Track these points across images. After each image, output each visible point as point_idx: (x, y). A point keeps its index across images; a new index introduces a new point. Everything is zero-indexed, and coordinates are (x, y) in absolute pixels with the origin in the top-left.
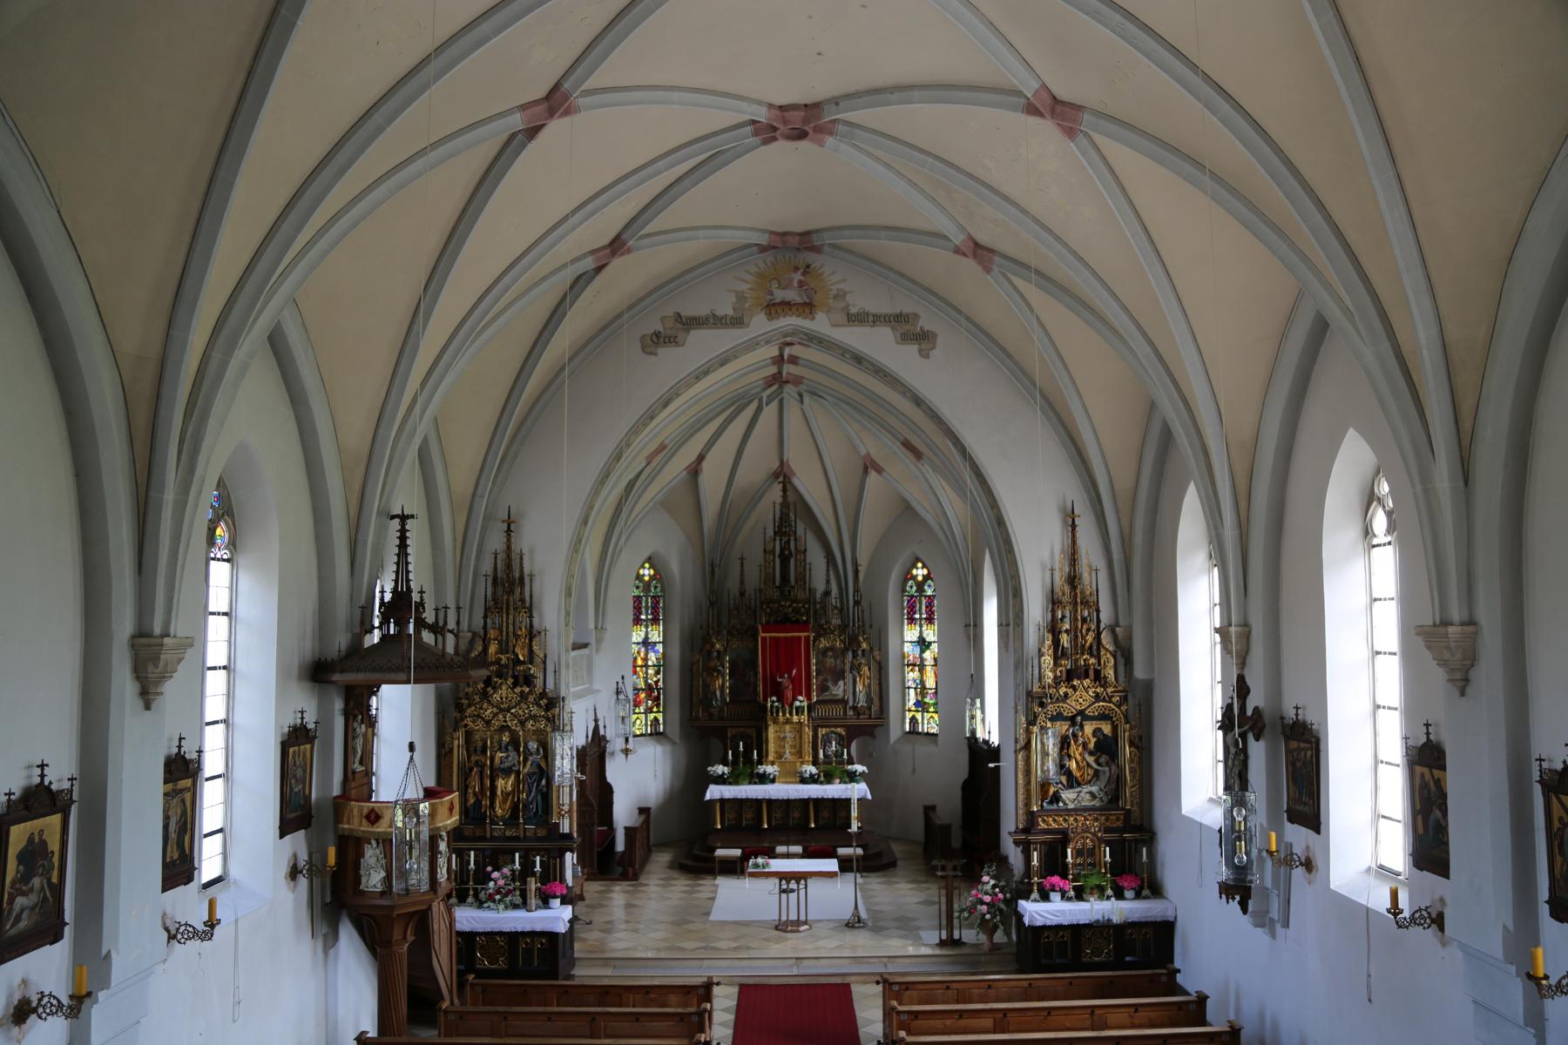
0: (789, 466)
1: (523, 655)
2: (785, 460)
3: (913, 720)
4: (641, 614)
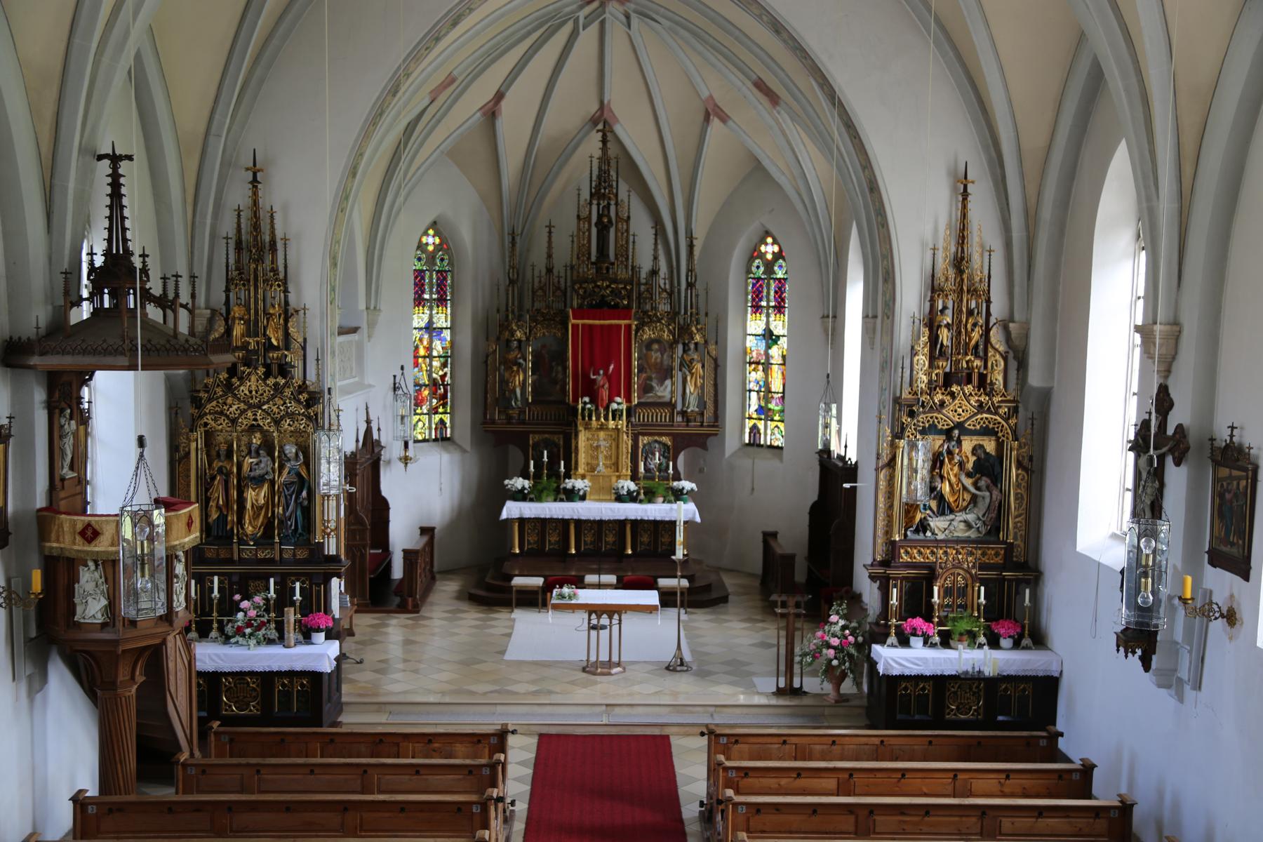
1: (277, 340)
2: (606, 102)
4: (423, 292)
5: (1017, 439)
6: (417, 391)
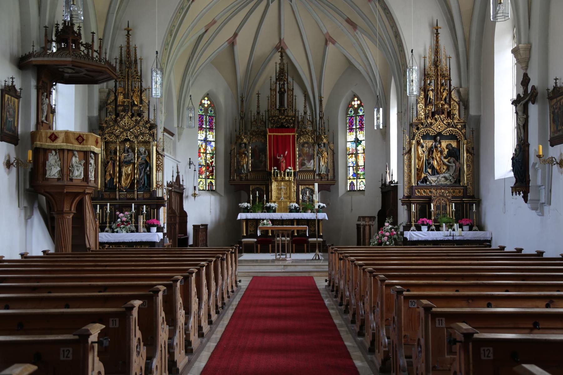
0: (284, 43)
1: (137, 102)
2: (282, 38)
3: (352, 184)
4: (203, 124)
5: (466, 139)
6: (200, 168)
